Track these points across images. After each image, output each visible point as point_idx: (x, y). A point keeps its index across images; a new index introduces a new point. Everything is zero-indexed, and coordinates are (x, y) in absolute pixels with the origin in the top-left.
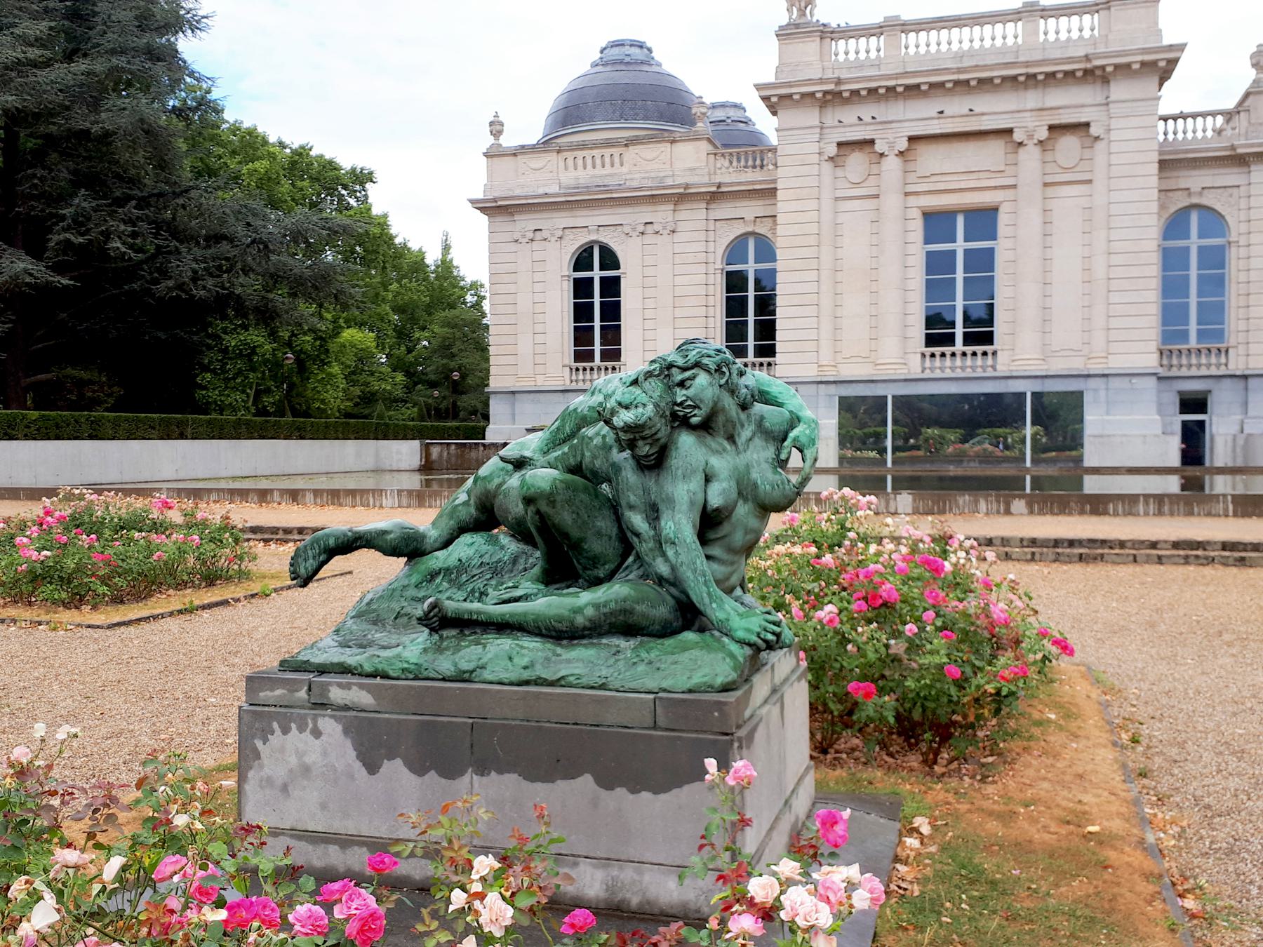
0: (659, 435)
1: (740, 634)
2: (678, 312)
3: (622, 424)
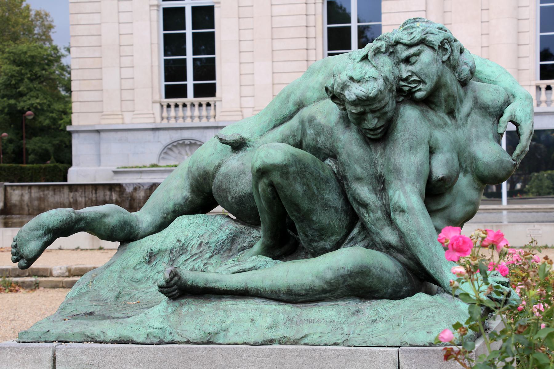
2: (278, 45)
3: (353, 97)
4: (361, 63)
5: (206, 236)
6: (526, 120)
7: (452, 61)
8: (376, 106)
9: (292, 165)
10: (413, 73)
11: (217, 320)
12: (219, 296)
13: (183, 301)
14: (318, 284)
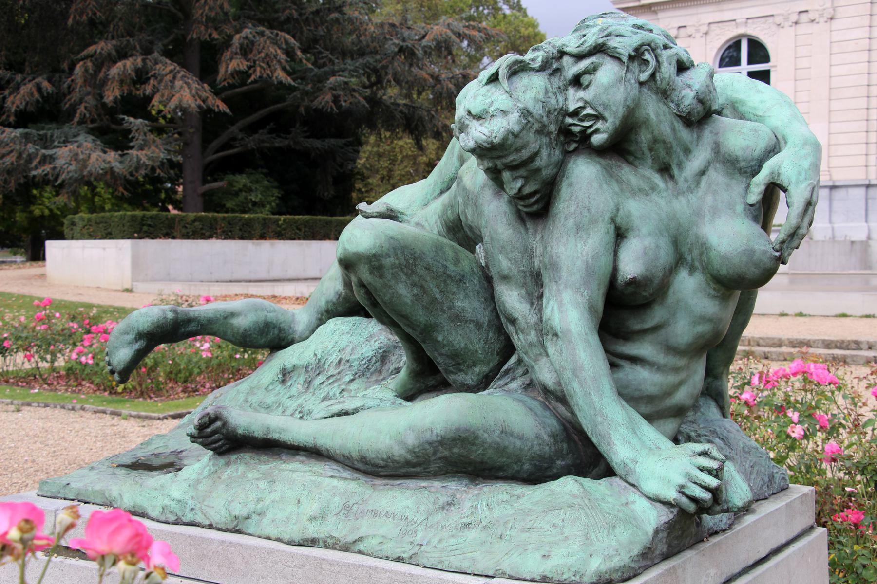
0: (539, 163)
1: (652, 487)
2: (835, 105)
4: (488, 87)
5: (349, 350)
6: (798, 182)
7: (659, 82)
8: (511, 158)
9: (388, 255)
10: (586, 102)
11: (253, 496)
12: (292, 451)
13: (234, 457)
14: (398, 452)
